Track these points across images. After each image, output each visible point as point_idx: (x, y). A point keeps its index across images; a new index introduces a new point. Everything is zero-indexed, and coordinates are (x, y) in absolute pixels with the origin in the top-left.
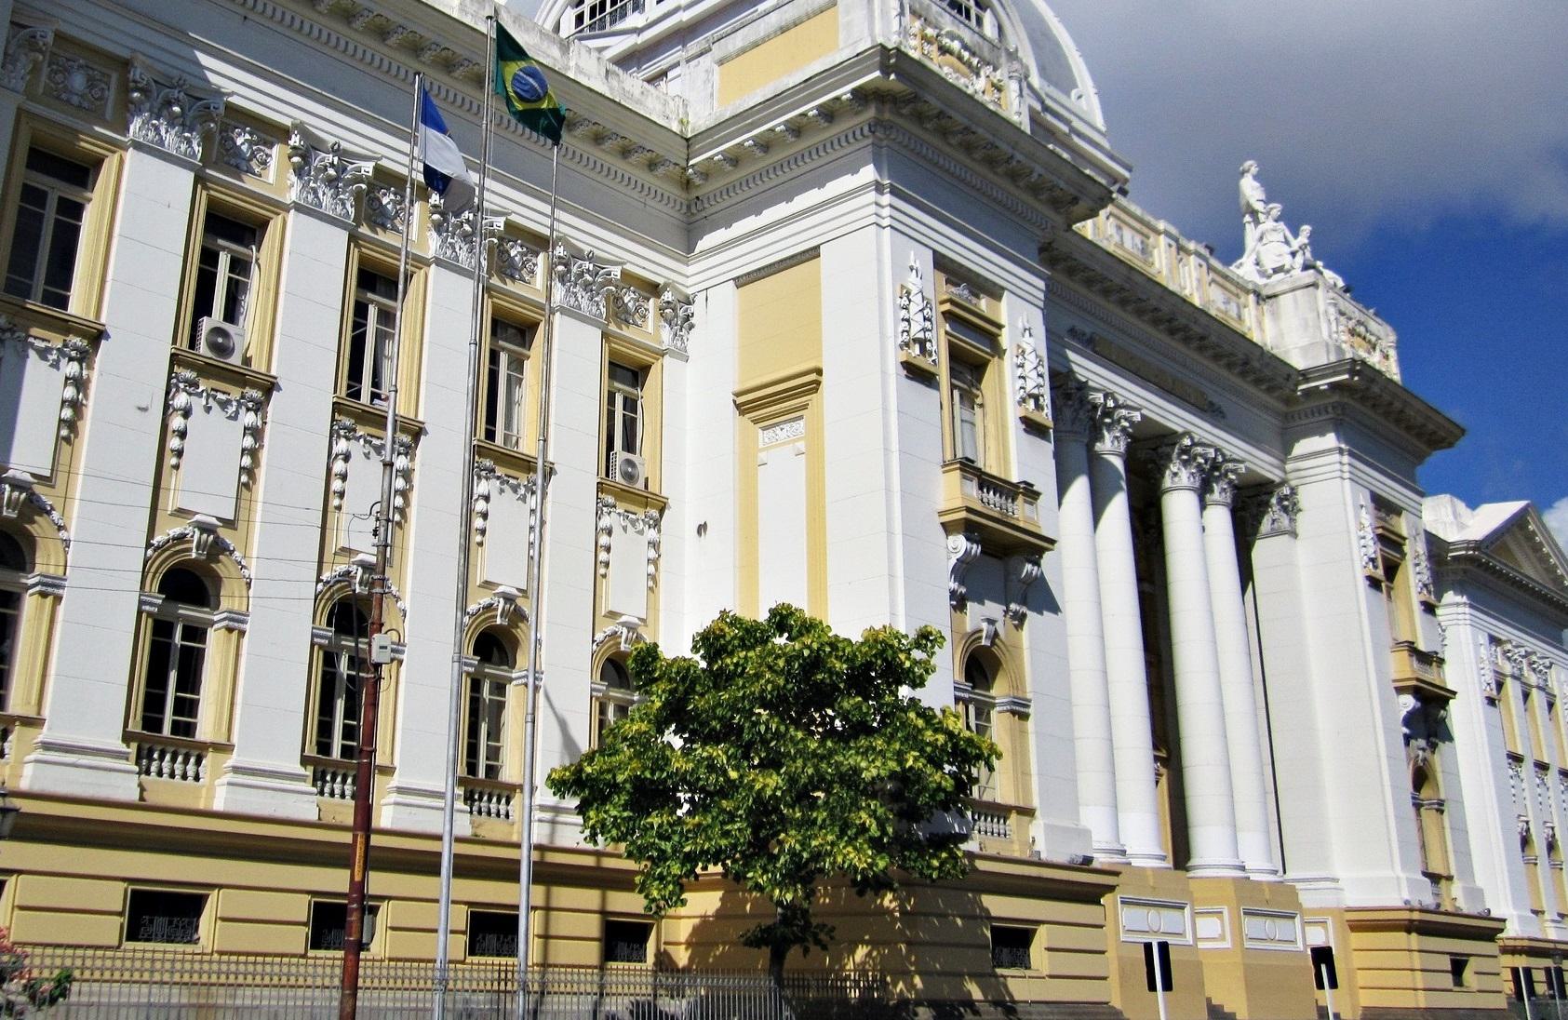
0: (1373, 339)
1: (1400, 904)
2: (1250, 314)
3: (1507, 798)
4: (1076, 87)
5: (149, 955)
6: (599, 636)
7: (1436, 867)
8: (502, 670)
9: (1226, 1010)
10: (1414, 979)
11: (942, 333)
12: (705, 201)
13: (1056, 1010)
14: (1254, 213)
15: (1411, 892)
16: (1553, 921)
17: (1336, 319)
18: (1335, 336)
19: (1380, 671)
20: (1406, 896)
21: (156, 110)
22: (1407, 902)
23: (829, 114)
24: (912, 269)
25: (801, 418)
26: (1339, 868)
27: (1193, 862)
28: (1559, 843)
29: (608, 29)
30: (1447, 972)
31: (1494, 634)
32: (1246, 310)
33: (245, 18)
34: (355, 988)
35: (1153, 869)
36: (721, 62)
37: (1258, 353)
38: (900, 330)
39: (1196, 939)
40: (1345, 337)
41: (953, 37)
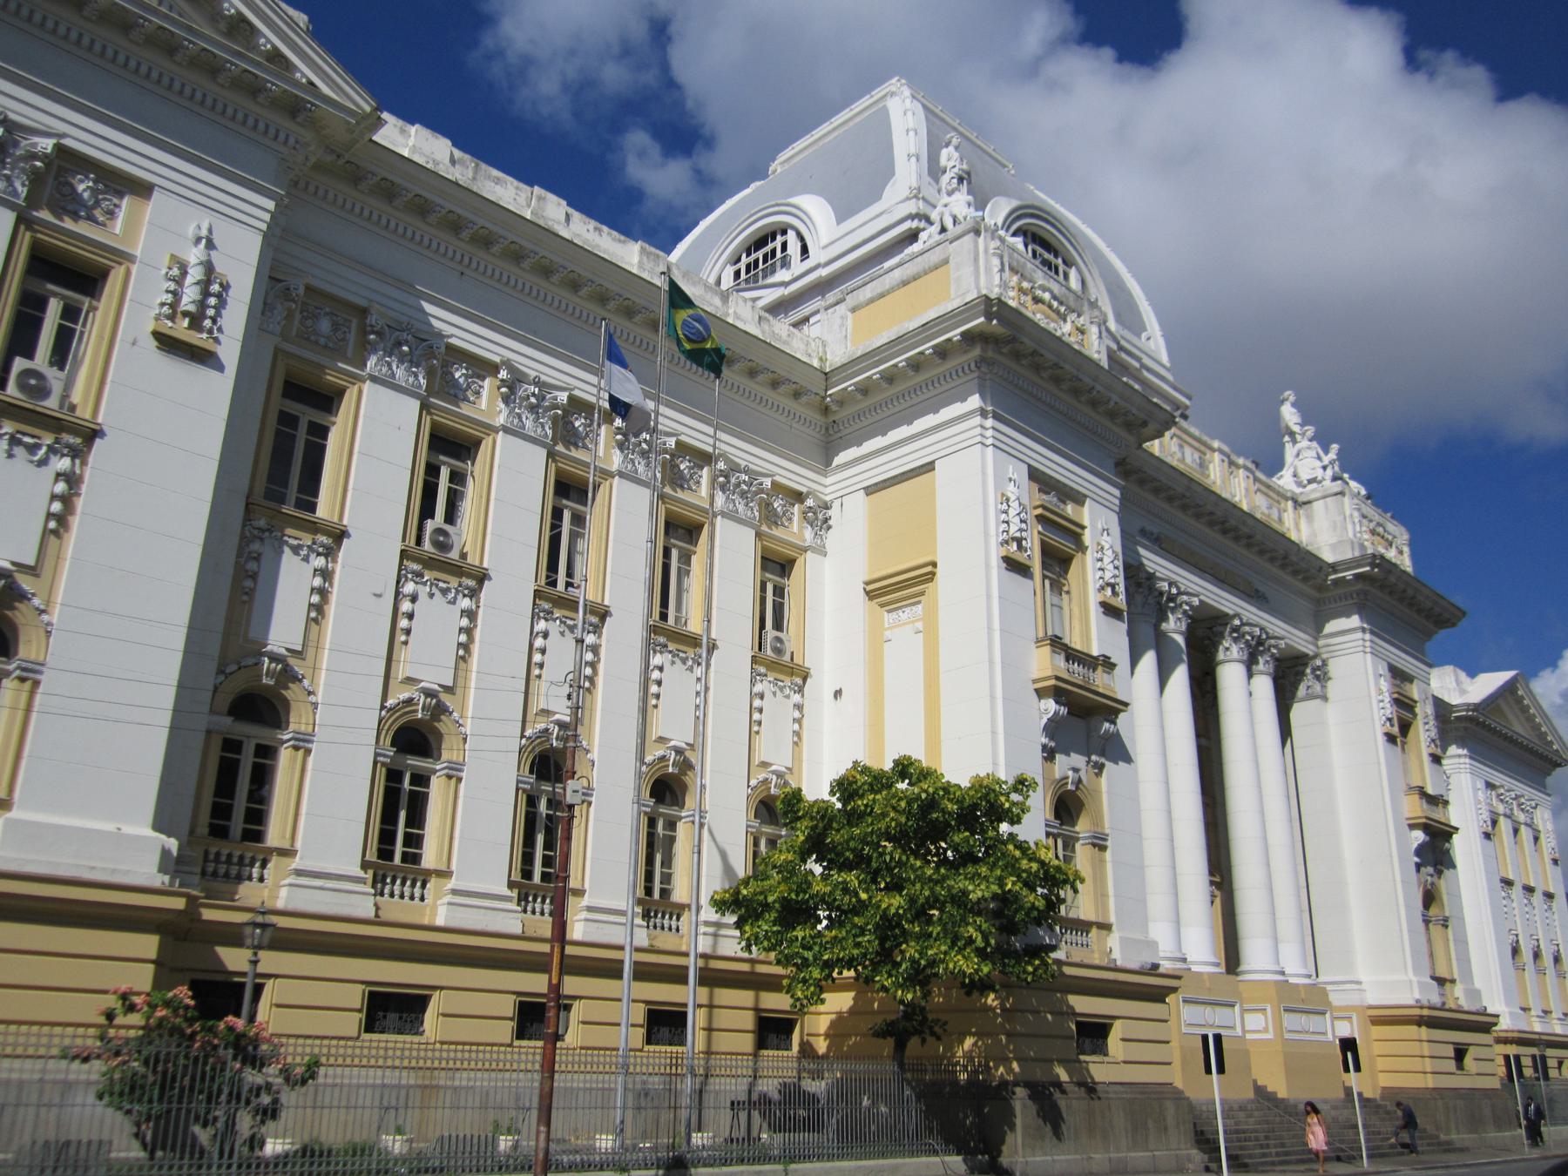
0: (1390, 538)
1: (1412, 1002)
7: (1442, 972)
9: (1269, 1089)
14: (1292, 434)
20: (1417, 996)
22: (1418, 1001)
25: (919, 602)
34: (553, 1072)
35: (1209, 974)
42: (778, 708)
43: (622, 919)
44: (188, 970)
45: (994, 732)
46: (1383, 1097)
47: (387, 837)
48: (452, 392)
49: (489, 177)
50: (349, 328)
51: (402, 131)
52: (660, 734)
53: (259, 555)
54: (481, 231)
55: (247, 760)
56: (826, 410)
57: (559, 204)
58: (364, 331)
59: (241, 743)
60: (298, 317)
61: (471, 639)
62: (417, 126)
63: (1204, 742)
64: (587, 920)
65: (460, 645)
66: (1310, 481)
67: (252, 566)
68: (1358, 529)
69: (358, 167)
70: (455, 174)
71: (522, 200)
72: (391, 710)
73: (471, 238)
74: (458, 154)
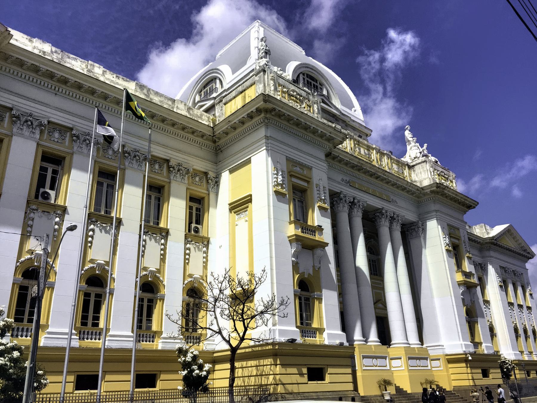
0: (447, 176)
1: (462, 352)
2: (406, 172)
3: (509, 317)
4: (354, 107)
5: (84, 394)
6: (186, 282)
7: (477, 340)
8: (82, 296)
9: (404, 390)
10: (468, 376)
11: (197, 172)
12: (220, 146)
13: (332, 394)
14: (409, 141)
15: (466, 348)
16: (527, 354)
17: (433, 171)
18: (433, 176)
19: (452, 279)
20: (464, 349)
21: (22, 123)
22: (464, 351)
23: (250, 116)
24: (278, 162)
25: (247, 210)
26: (443, 341)
27: (392, 343)
28: (519, 328)
29: (208, 98)
30: (481, 373)
31: (501, 265)
32: (405, 171)
33: (56, 94)
34: (233, 395)
35: (375, 345)
36: (225, 104)
37: (406, 183)
38: (274, 181)
39: (432, 367)
40: (437, 177)
41: (294, 91)
42: (196, 256)
43: (67, 337)
44: (76, 372)
45: (271, 257)
46: (454, 390)
47: (140, 321)
48: (195, 183)
49: (69, 58)
50: (164, 166)
51: (30, 41)
52: (91, 258)
53: (33, 219)
54: (62, 78)
55: (92, 299)
56: (215, 142)
57: (100, 68)
58: (169, 167)
59: (102, 294)
60: (101, 150)
61: (207, 260)
62: (36, 38)
63: (374, 257)
64: (162, 342)
65: (161, 255)
66: (415, 158)
67: (30, 222)
68: (433, 174)
69: (6, 54)
70: (55, 57)
71: (84, 66)
72: (22, 262)
73: (12, 62)
74: (54, 49)
